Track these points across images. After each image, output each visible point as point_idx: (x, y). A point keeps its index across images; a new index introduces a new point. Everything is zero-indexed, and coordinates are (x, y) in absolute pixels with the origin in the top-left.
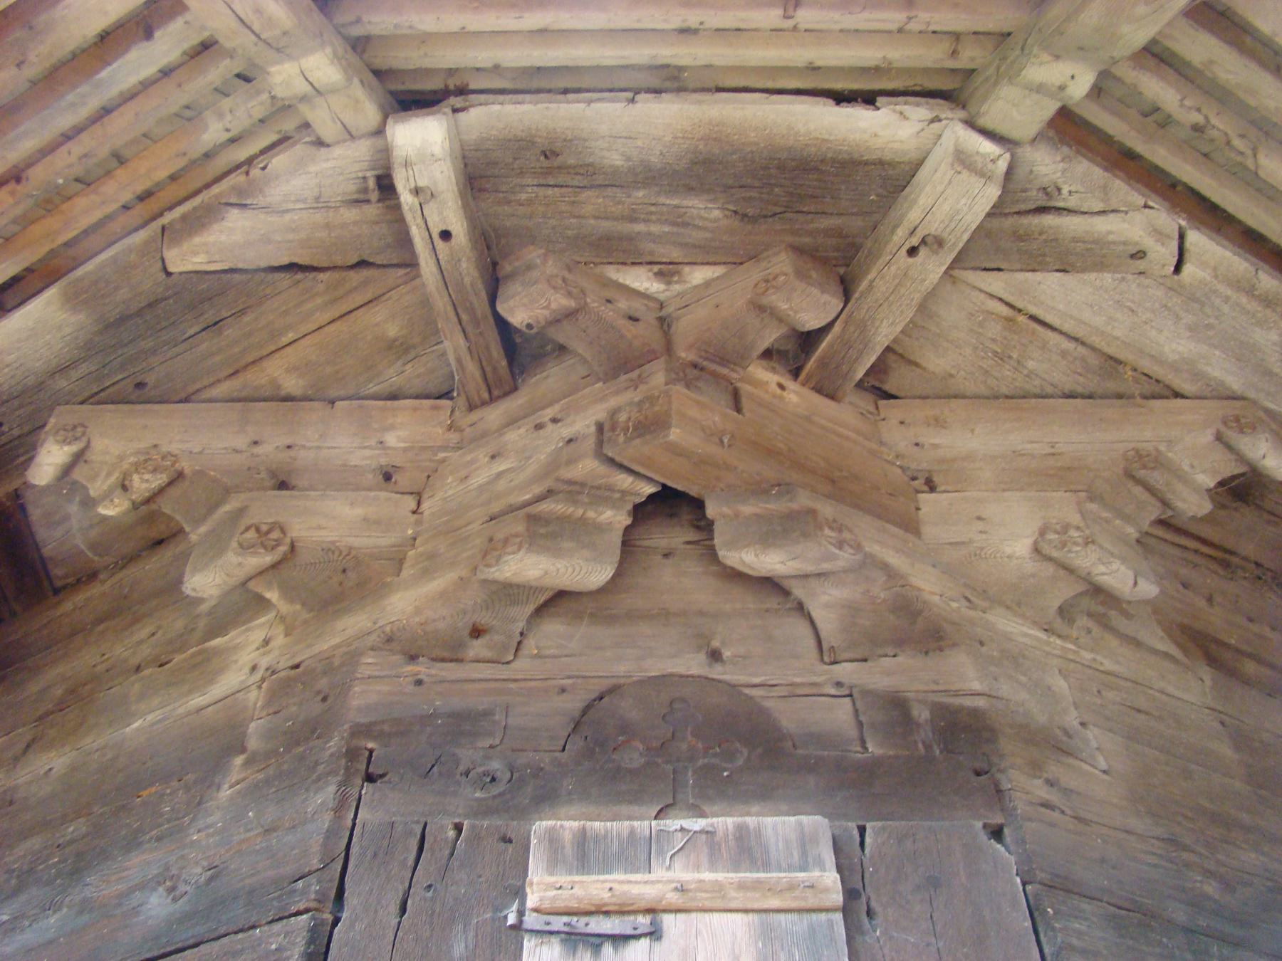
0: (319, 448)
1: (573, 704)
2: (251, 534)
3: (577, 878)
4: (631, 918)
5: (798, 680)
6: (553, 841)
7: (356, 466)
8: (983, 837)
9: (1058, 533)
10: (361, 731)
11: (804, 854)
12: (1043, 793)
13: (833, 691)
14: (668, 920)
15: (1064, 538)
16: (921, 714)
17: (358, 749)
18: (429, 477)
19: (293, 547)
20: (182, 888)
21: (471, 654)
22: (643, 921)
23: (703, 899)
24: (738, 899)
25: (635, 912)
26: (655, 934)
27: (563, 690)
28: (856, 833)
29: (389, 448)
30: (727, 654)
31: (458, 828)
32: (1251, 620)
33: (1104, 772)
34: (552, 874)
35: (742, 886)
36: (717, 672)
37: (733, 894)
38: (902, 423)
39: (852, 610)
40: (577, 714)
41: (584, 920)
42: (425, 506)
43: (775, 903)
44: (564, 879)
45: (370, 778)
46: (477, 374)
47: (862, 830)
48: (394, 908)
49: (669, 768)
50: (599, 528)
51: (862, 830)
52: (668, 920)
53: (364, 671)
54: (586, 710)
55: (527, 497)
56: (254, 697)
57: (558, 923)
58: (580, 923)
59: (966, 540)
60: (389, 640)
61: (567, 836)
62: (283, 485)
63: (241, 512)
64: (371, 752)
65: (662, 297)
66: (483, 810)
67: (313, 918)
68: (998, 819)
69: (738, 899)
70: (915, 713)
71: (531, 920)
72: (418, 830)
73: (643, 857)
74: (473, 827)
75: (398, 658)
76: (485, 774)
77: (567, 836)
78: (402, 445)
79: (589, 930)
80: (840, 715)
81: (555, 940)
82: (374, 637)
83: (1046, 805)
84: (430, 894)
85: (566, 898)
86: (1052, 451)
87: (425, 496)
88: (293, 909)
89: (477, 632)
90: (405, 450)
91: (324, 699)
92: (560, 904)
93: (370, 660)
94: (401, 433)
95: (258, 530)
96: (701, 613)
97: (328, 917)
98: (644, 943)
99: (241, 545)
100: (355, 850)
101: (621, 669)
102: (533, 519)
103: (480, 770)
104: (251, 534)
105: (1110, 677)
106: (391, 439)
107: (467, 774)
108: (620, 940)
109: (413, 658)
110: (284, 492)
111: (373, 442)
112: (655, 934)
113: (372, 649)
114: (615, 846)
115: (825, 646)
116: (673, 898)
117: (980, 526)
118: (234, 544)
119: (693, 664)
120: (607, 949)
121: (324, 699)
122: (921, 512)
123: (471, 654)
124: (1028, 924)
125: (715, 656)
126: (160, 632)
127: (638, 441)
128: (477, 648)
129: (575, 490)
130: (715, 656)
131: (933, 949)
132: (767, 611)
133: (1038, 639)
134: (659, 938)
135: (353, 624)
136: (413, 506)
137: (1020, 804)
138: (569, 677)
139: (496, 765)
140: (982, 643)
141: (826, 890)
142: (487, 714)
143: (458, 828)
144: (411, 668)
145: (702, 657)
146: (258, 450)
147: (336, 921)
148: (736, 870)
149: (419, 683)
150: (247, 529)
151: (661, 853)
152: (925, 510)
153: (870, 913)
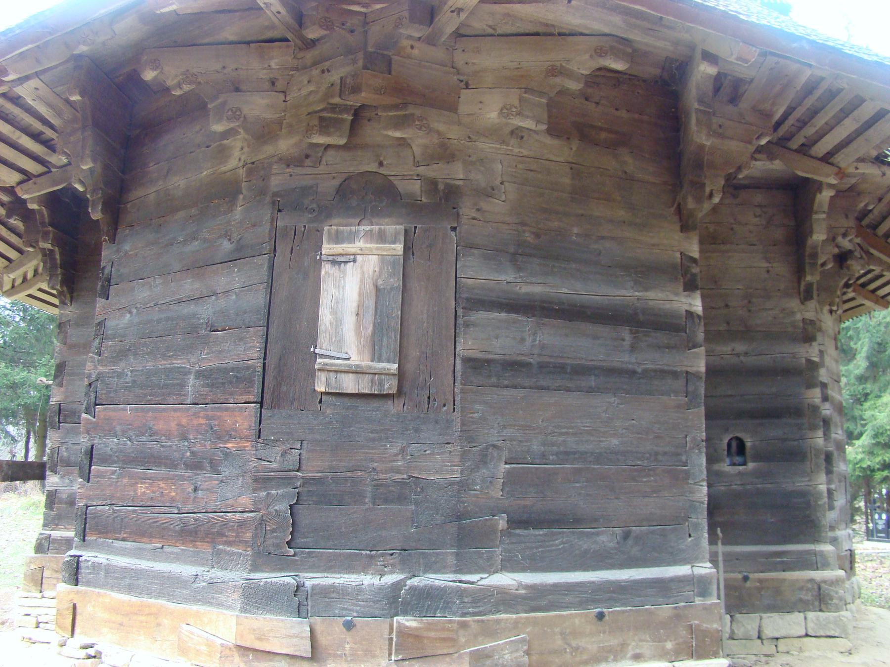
0: (247, 69)
1: (336, 183)
2: (230, 113)
3: (335, 246)
4: (349, 257)
5: (406, 173)
6: (329, 232)
7: (261, 78)
8: (449, 230)
9: (507, 109)
10: (275, 194)
11: (396, 238)
12: (474, 214)
13: (416, 178)
14: (358, 257)
15: (510, 112)
16: (441, 187)
17: (275, 201)
18: (288, 83)
19: (245, 117)
20: (233, 240)
21: (306, 164)
22: (352, 257)
23: (367, 252)
24: (375, 252)
25: (350, 255)
26: (354, 261)
27: (334, 178)
28: (413, 228)
29: (273, 69)
30: (385, 163)
31: (305, 226)
32: (617, 109)
33: (503, 201)
34: (329, 244)
35: (377, 249)
36: (382, 171)
37: (374, 251)
38: (463, 51)
39: (426, 147)
40: (338, 187)
41: (337, 257)
42: (288, 99)
43: (385, 253)
44: (332, 246)
45: (279, 211)
46: (300, 42)
47: (415, 228)
48: (289, 252)
49: (363, 206)
50: (343, 120)
51: (415, 228)
52: (358, 257)
53: (274, 171)
54: (340, 185)
55: (319, 109)
56: (242, 172)
57: (331, 258)
58: (336, 258)
59: (473, 113)
60: (281, 159)
61: (333, 231)
62: (237, 90)
63: (224, 104)
64: (279, 201)
65: (366, 12)
66: (311, 221)
67: (269, 256)
68: (455, 225)
69: (375, 252)
70: (439, 187)
71: (323, 257)
72: (294, 228)
73: (353, 238)
74: (308, 227)
75: (283, 166)
76: (312, 209)
77: (333, 231)
78: (277, 67)
79: (338, 260)
80: (416, 187)
81: (330, 262)
82: (275, 158)
83: (474, 219)
84: (298, 248)
85: (332, 252)
86: (519, 66)
87: (287, 93)
88: (264, 253)
89: (307, 156)
90: (278, 69)
91: (263, 180)
92: (330, 253)
93: (275, 167)
94: (276, 61)
95: (232, 111)
96: (379, 146)
97: (273, 255)
98: (352, 263)
99: (228, 119)
100: (277, 235)
101: (352, 169)
102: (322, 119)
103: (310, 207)
104: (230, 113)
105: (524, 158)
106: (273, 64)
107: (307, 208)
108: (346, 262)
109: (288, 166)
110: (239, 93)
111: (266, 66)
112: (354, 261)
113: (276, 162)
114: (346, 234)
115: (416, 160)
116: (359, 252)
117: (480, 106)
118: (225, 118)
119: (373, 167)
120: (342, 265)
121: (263, 180)
122: (460, 99)
123: (306, 164)
124: (455, 259)
125: (381, 164)
126: (203, 130)
127: (352, 95)
128: (308, 162)
129: (333, 108)
130: (381, 164)
131: (428, 265)
132: (400, 145)
133: (496, 148)
134: (356, 262)
135: (269, 150)
136: (283, 98)
137: (464, 220)
138: (336, 173)
139: (314, 206)
140: (470, 156)
141: (399, 251)
142: (312, 187)
143: (305, 226)
144: (288, 170)
145: (377, 164)
146: (226, 71)
147: (275, 256)
148: (377, 243)
149: (291, 176)
150: (228, 111)
151: (358, 237)
152: (462, 97)
153: (413, 254)
